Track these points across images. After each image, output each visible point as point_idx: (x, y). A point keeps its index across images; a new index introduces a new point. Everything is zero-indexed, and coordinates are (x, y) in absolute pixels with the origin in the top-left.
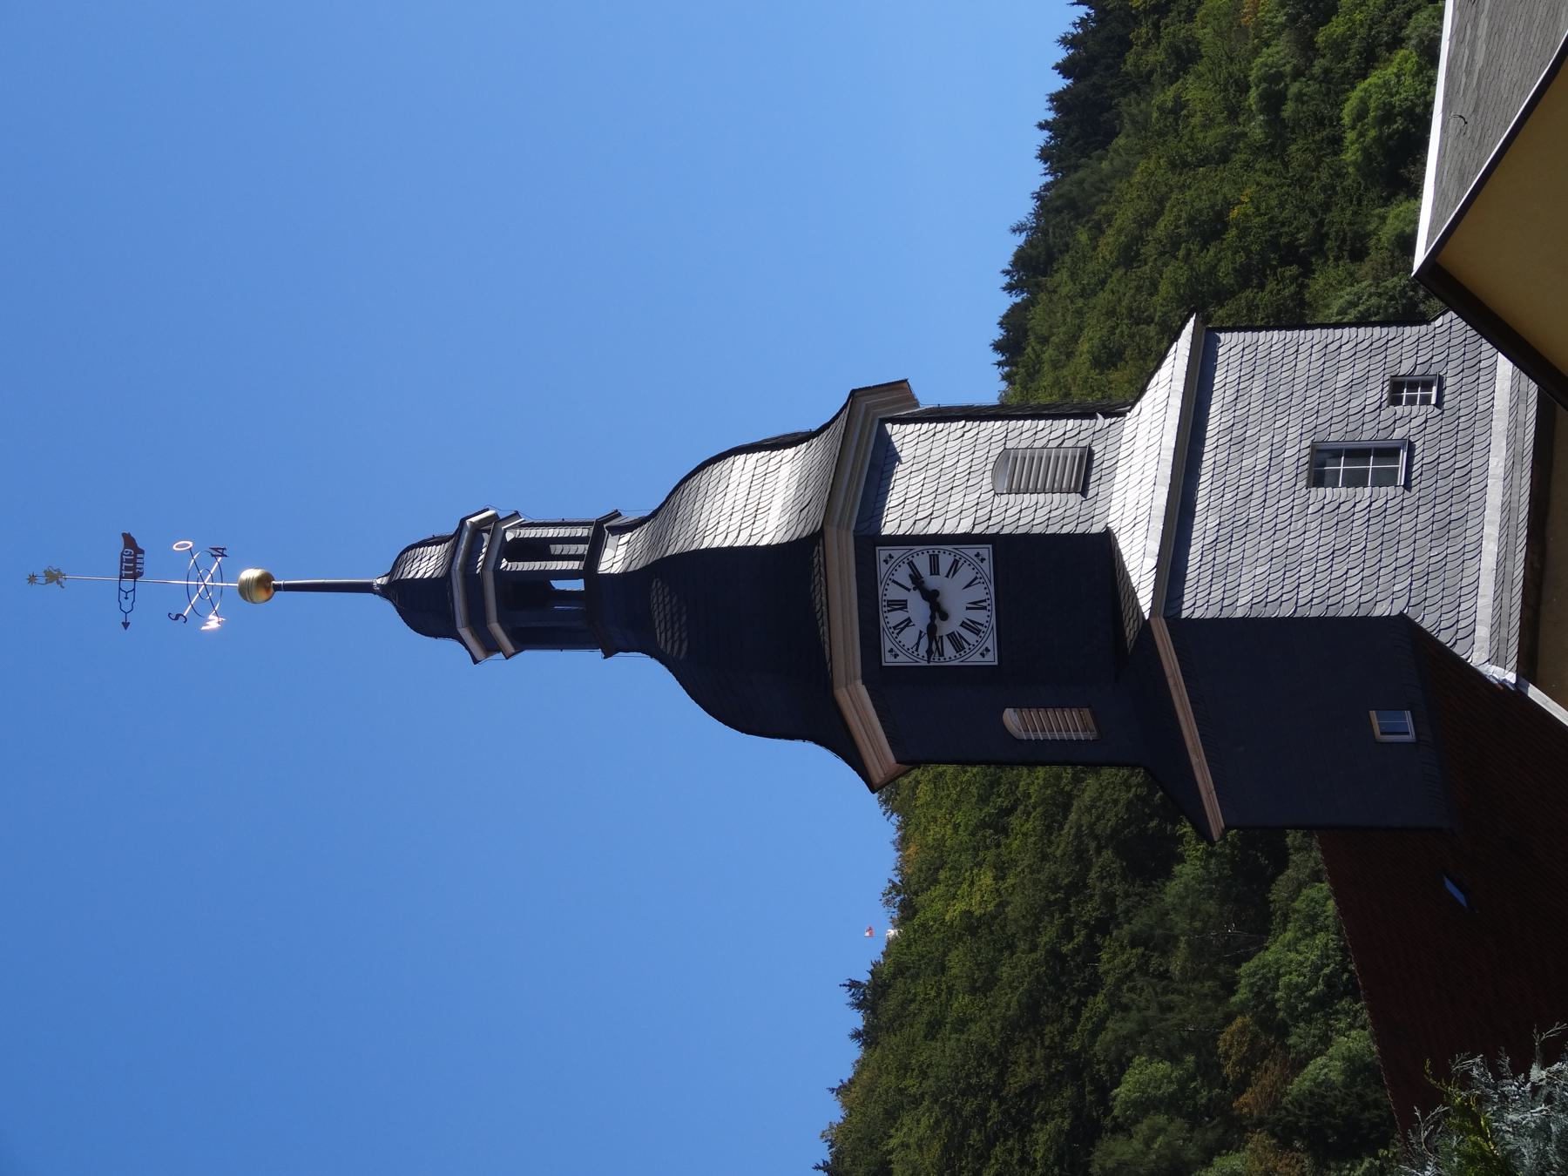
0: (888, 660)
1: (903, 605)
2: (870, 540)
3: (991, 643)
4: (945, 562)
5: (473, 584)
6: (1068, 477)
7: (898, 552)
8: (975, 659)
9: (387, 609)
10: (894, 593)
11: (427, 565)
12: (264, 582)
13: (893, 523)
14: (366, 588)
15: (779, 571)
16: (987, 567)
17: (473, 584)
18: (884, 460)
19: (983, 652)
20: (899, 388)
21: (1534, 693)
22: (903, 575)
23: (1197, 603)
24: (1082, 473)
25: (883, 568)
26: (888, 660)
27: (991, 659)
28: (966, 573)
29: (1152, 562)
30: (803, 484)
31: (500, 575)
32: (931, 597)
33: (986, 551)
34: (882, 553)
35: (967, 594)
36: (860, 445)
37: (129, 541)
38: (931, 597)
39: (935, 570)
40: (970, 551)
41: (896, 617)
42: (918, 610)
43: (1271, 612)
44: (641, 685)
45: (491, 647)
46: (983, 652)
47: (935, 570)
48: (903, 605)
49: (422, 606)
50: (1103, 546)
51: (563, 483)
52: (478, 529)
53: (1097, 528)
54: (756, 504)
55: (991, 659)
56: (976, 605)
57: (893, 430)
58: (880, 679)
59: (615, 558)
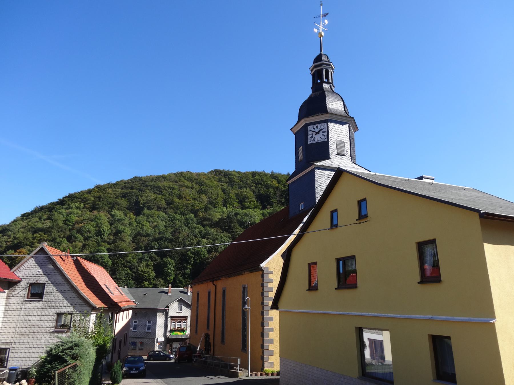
0: (309, 127)
1: (317, 128)
2: (327, 121)
3: (312, 142)
4: (324, 134)
5: (321, 65)
6: (339, 152)
7: (326, 126)
8: (309, 140)
9: (319, 54)
10: (319, 126)
11: (324, 58)
12: (321, 36)
13: (329, 124)
14: (321, 51)
15: (324, 109)
16: (324, 140)
17: (321, 65)
18: (343, 124)
19: (310, 141)
20: (356, 129)
21: (302, 225)
22: (322, 127)
23: (317, 172)
24: (341, 154)
25: (323, 124)
26: (309, 127)
27: (309, 143)
28: (323, 137)
29: (324, 165)
30: (337, 111)
31: (323, 69)
32: (318, 133)
33: (326, 140)
34: (326, 124)
35: (320, 138)
36: (344, 119)
37: (327, 14)
38: (318, 133)
39: (323, 132)
40: (326, 137)
41: (315, 127)
42: (317, 130)
43: (316, 183)
44: (307, 92)
45: (312, 71)
46: (310, 141)
47: (323, 132)
48: (317, 128)
49: (319, 58)
50: (327, 157)
51: (339, 76)
52: (330, 65)
53: (330, 157)
54: (334, 105)
55: (309, 143)
56: (318, 139)
57: (347, 125)
58: (306, 125)
59: (326, 86)
